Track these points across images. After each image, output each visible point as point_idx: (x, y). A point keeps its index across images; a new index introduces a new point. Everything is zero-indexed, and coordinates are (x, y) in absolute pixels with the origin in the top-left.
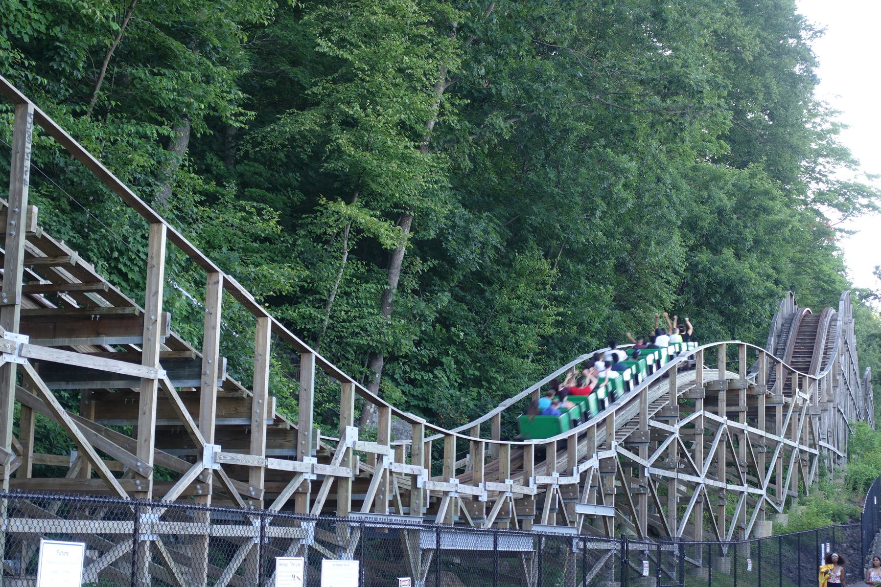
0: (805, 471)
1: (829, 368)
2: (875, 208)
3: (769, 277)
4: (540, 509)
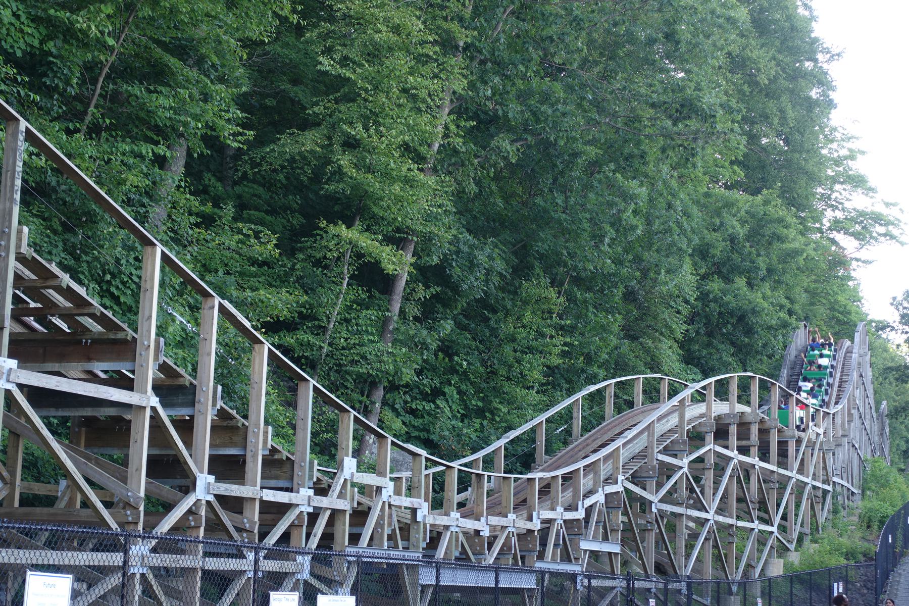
2: (892, 237)
3: (782, 307)
4: (544, 544)
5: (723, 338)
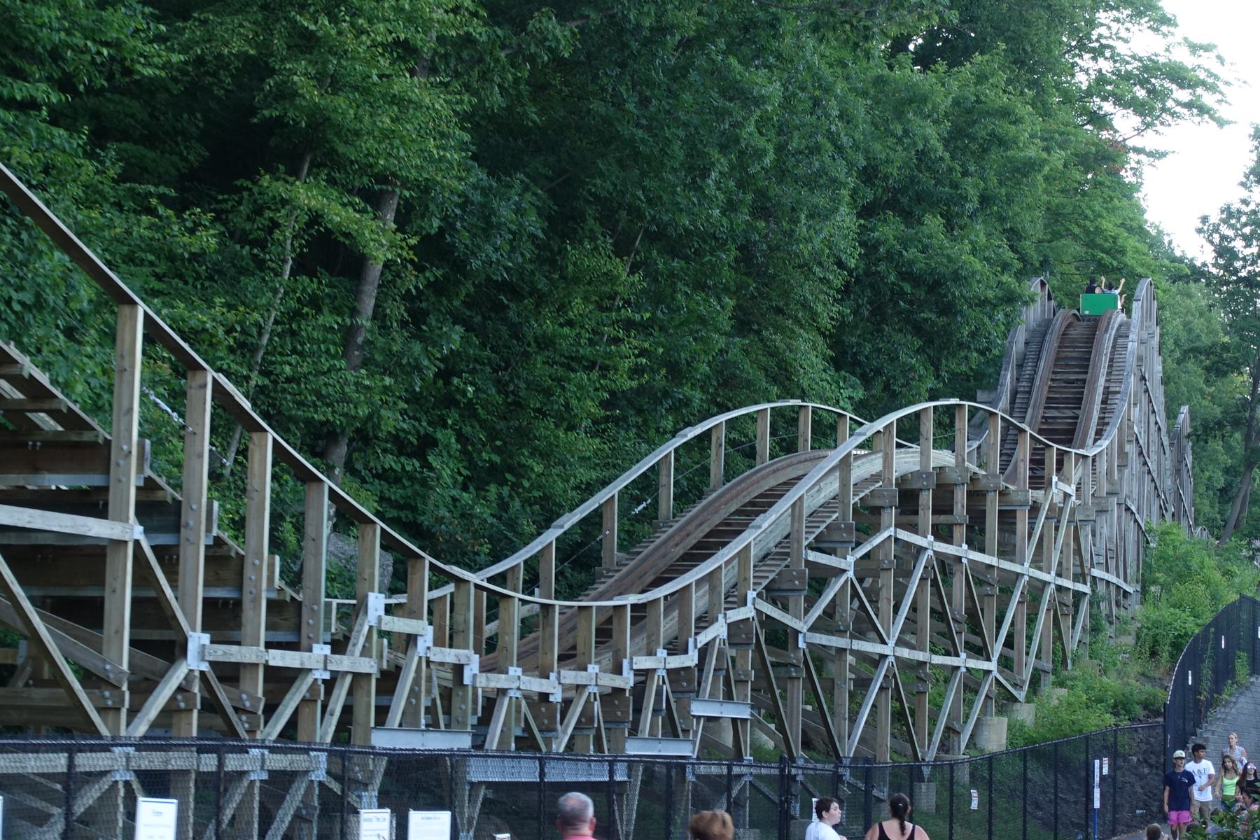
0: (1065, 623)
1: (1112, 433)
2: (1203, 110)
3: (1005, 266)
4: (638, 710)
5: (907, 332)
